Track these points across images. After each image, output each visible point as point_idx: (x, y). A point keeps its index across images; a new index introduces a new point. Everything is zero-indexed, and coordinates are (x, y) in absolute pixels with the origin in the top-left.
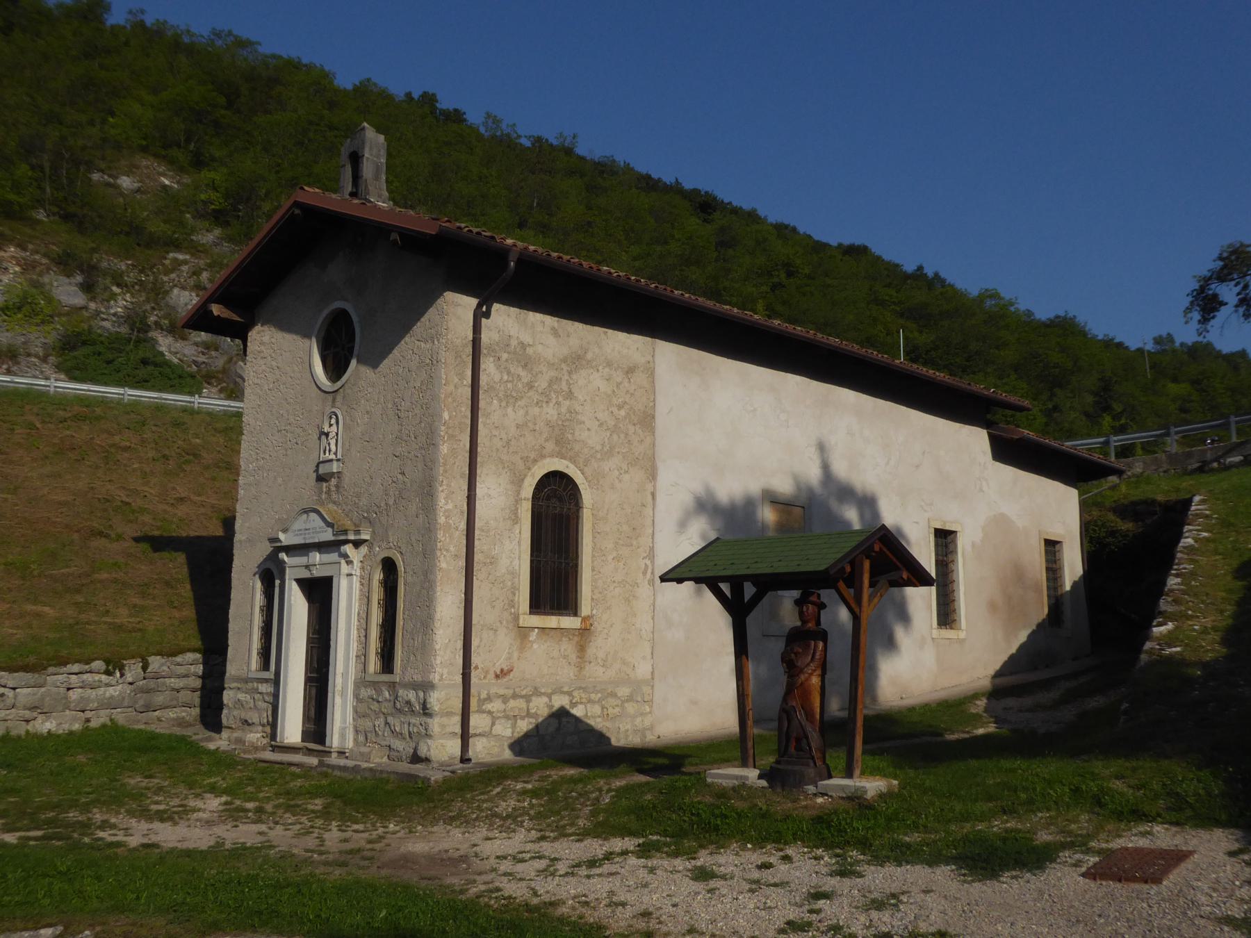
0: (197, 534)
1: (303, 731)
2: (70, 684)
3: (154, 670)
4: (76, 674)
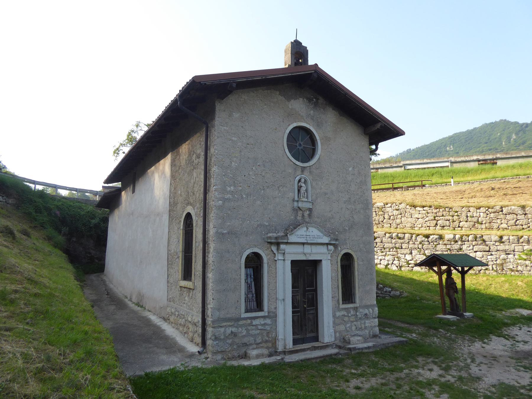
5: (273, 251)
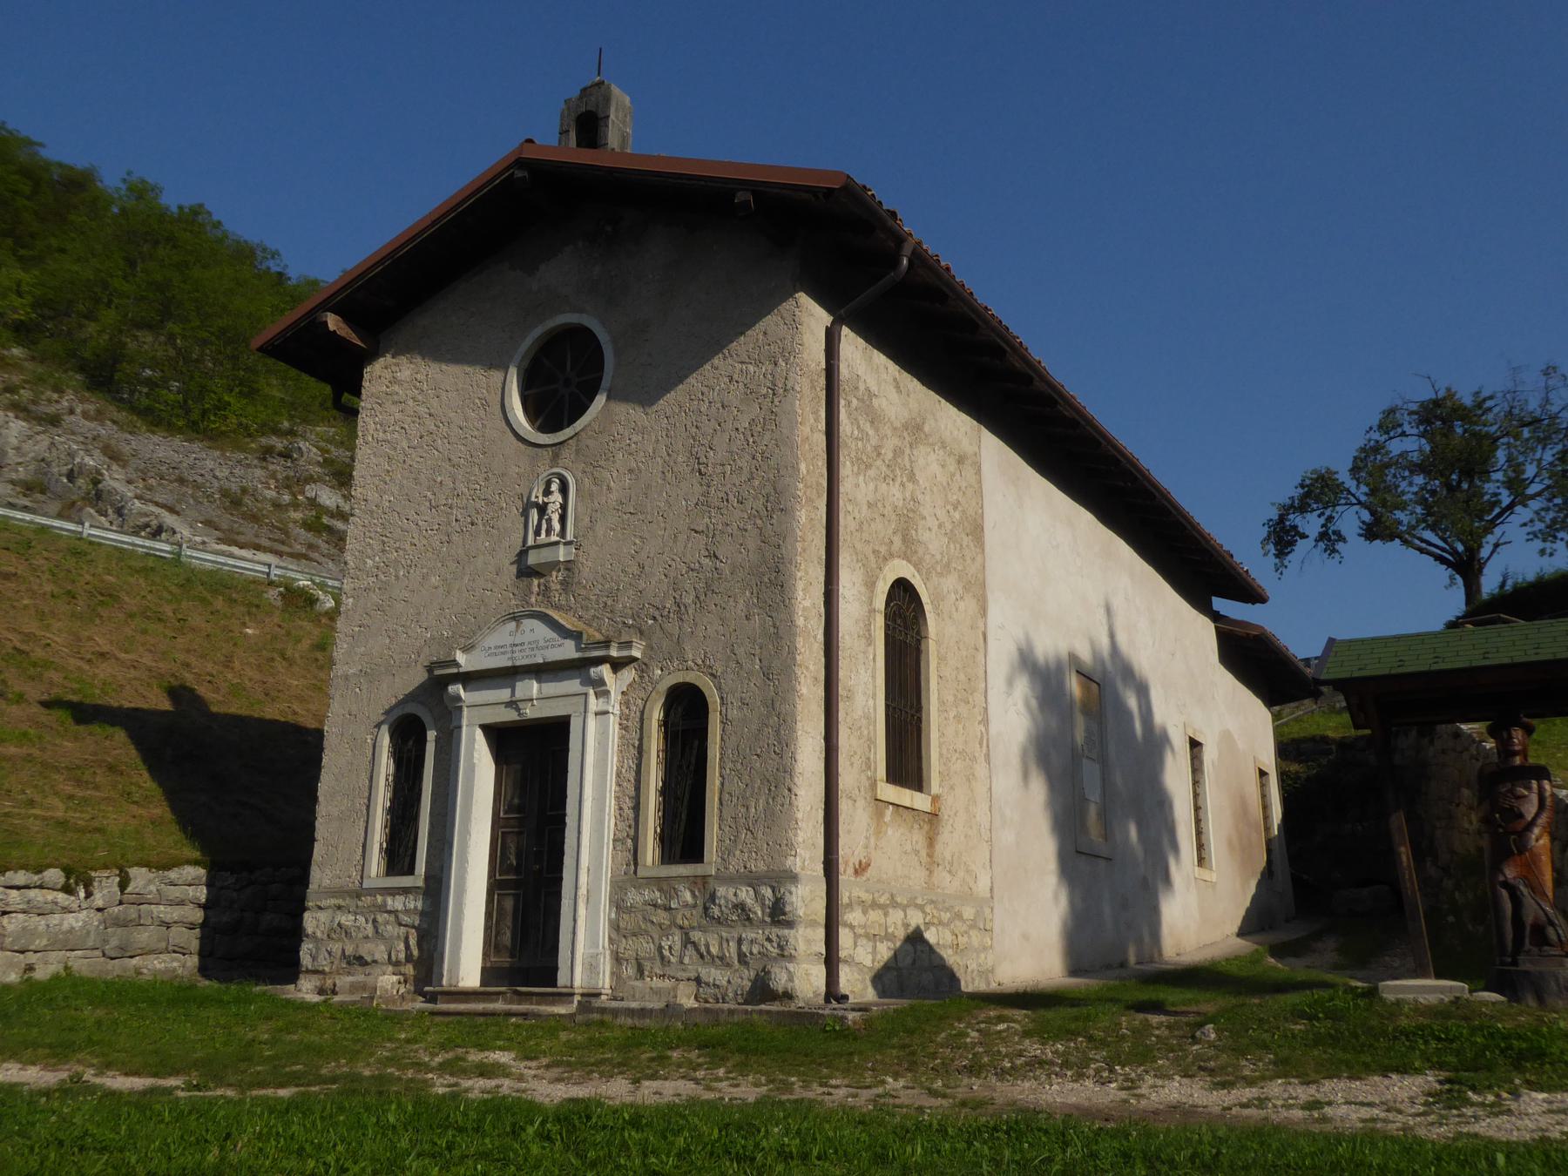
0: (132, 705)
1: (483, 970)
2: (7, 905)
3: (137, 890)
4: (18, 888)
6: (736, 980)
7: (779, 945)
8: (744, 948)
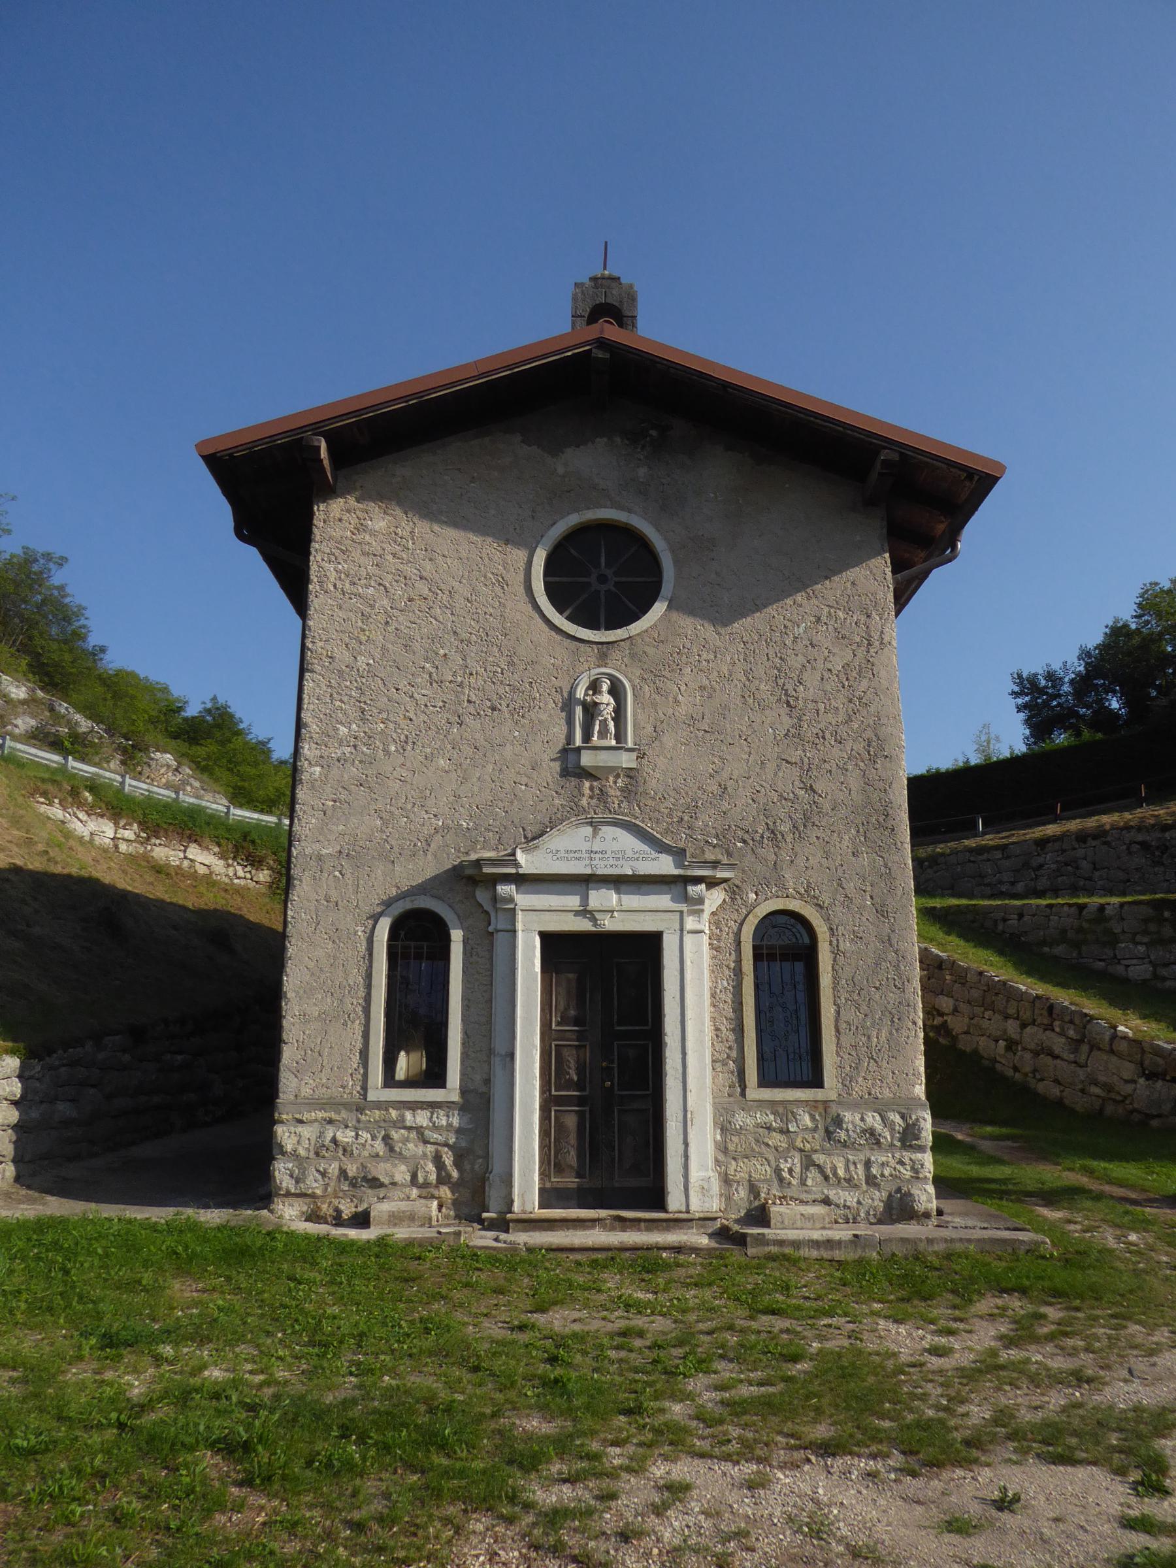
5: (481, 906)
6: (867, 1201)
7: (913, 1168)
8: (874, 1171)
